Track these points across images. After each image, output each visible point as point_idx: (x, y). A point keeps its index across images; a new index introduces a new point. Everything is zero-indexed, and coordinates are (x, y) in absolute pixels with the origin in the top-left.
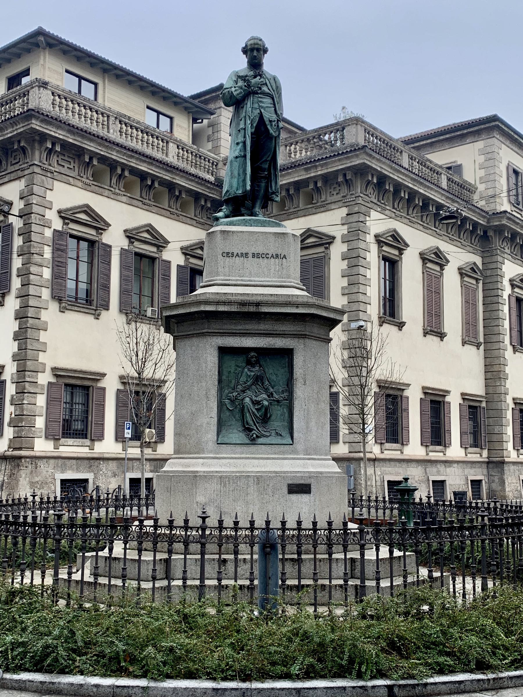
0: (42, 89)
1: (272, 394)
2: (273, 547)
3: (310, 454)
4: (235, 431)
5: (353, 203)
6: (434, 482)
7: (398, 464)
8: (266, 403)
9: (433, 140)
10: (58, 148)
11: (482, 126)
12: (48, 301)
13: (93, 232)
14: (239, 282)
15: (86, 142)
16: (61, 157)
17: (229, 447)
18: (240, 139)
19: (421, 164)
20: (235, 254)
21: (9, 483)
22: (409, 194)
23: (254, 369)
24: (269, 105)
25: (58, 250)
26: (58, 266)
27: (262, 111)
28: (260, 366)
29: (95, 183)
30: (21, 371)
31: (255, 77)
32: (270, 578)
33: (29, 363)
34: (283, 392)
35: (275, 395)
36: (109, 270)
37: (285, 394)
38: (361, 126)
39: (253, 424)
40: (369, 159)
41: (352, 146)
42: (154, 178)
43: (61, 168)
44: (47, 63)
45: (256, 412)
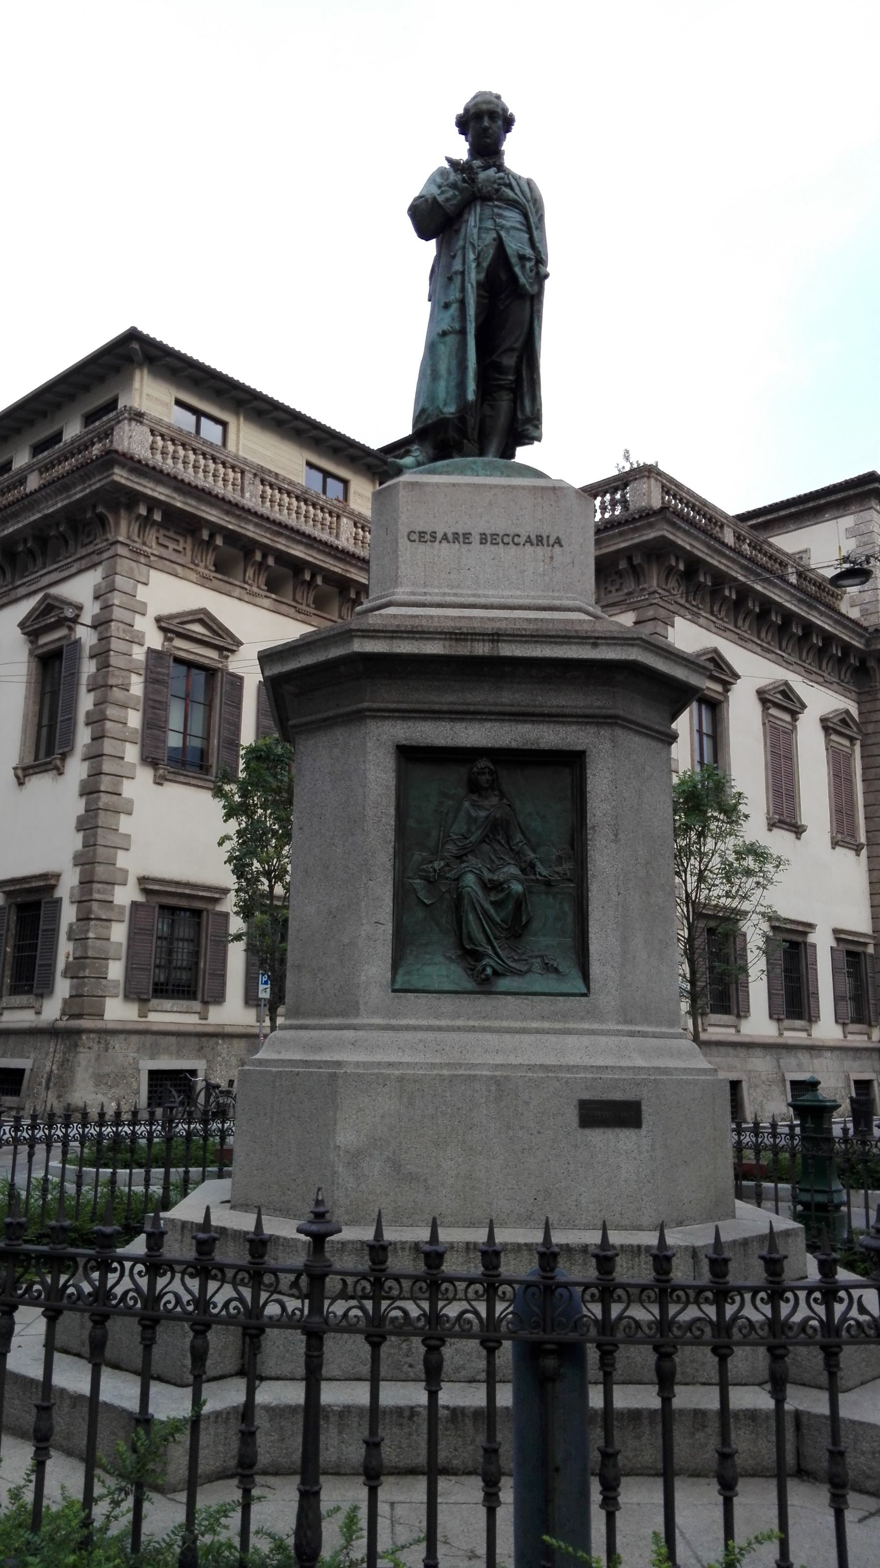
0: (134, 423)
1: (533, 866)
2: (571, 1353)
3: (618, 1027)
4: (439, 958)
5: (647, 603)
6: (794, 1083)
7: (731, 1051)
8: (517, 887)
9: (769, 517)
10: (157, 517)
11: (851, 492)
12: (134, 765)
13: (214, 654)
14: (448, 599)
15: (203, 508)
16: (162, 532)
17: (423, 998)
18: (454, 294)
19: (754, 548)
20: (439, 536)
21: (60, 1077)
22: (738, 593)
23: (486, 803)
24: (518, 226)
25: (156, 681)
26: (153, 708)
27: (503, 233)
28: (502, 795)
29: (220, 576)
30: (87, 882)
31: (485, 168)
32: (557, 1470)
33: (99, 869)
34: (560, 860)
35: (540, 868)
36: (239, 716)
37: (567, 866)
38: (656, 480)
39: (484, 941)
40: (670, 529)
41: (640, 511)
42: (316, 570)
43: (162, 550)
44: (145, 386)
45: (492, 911)
